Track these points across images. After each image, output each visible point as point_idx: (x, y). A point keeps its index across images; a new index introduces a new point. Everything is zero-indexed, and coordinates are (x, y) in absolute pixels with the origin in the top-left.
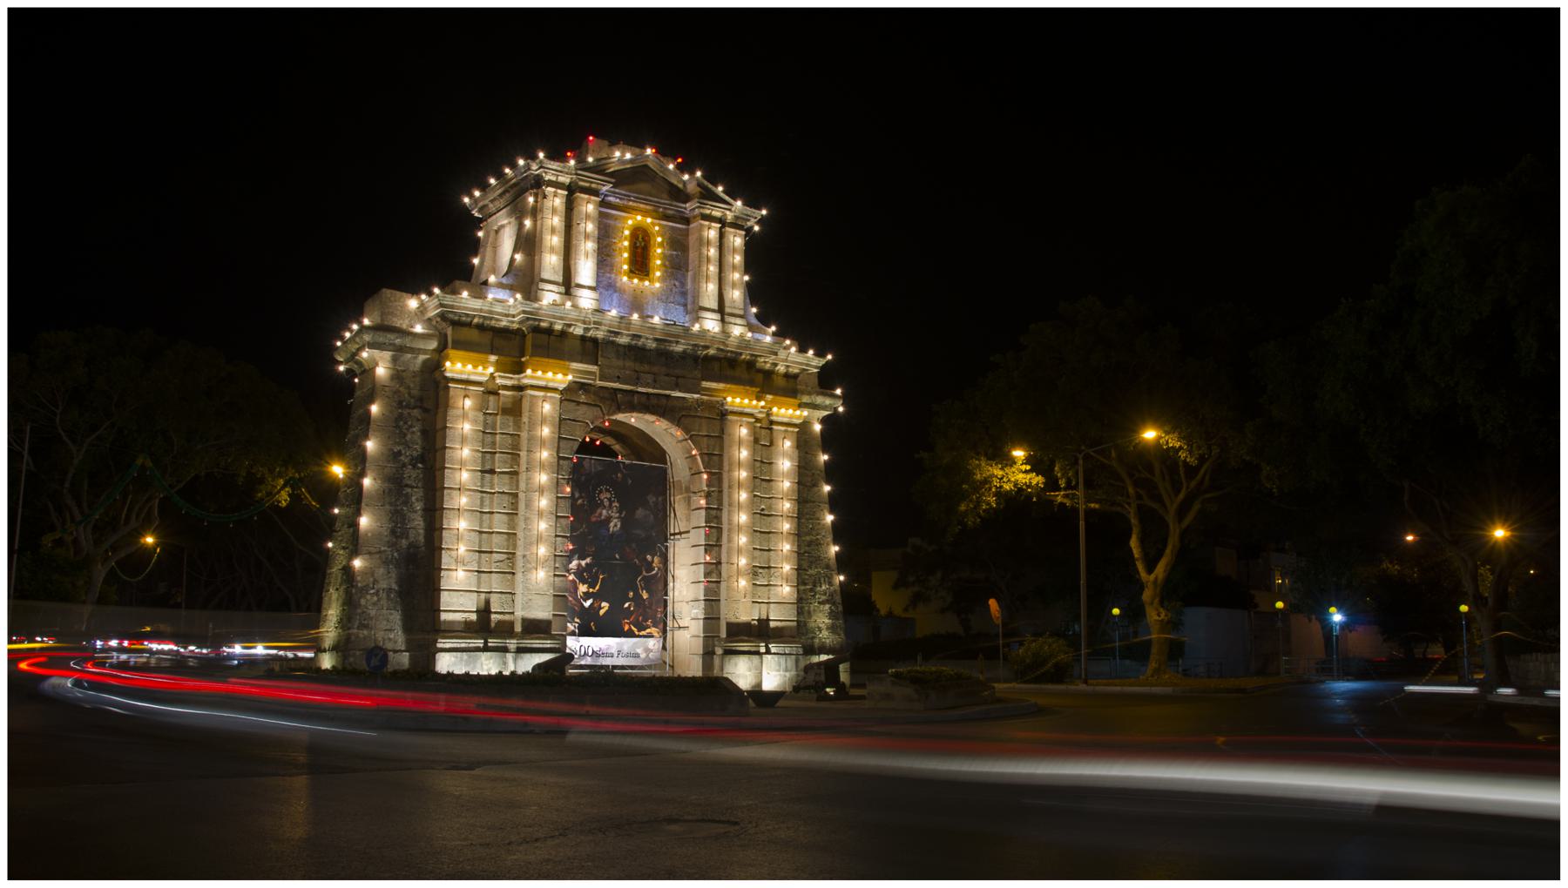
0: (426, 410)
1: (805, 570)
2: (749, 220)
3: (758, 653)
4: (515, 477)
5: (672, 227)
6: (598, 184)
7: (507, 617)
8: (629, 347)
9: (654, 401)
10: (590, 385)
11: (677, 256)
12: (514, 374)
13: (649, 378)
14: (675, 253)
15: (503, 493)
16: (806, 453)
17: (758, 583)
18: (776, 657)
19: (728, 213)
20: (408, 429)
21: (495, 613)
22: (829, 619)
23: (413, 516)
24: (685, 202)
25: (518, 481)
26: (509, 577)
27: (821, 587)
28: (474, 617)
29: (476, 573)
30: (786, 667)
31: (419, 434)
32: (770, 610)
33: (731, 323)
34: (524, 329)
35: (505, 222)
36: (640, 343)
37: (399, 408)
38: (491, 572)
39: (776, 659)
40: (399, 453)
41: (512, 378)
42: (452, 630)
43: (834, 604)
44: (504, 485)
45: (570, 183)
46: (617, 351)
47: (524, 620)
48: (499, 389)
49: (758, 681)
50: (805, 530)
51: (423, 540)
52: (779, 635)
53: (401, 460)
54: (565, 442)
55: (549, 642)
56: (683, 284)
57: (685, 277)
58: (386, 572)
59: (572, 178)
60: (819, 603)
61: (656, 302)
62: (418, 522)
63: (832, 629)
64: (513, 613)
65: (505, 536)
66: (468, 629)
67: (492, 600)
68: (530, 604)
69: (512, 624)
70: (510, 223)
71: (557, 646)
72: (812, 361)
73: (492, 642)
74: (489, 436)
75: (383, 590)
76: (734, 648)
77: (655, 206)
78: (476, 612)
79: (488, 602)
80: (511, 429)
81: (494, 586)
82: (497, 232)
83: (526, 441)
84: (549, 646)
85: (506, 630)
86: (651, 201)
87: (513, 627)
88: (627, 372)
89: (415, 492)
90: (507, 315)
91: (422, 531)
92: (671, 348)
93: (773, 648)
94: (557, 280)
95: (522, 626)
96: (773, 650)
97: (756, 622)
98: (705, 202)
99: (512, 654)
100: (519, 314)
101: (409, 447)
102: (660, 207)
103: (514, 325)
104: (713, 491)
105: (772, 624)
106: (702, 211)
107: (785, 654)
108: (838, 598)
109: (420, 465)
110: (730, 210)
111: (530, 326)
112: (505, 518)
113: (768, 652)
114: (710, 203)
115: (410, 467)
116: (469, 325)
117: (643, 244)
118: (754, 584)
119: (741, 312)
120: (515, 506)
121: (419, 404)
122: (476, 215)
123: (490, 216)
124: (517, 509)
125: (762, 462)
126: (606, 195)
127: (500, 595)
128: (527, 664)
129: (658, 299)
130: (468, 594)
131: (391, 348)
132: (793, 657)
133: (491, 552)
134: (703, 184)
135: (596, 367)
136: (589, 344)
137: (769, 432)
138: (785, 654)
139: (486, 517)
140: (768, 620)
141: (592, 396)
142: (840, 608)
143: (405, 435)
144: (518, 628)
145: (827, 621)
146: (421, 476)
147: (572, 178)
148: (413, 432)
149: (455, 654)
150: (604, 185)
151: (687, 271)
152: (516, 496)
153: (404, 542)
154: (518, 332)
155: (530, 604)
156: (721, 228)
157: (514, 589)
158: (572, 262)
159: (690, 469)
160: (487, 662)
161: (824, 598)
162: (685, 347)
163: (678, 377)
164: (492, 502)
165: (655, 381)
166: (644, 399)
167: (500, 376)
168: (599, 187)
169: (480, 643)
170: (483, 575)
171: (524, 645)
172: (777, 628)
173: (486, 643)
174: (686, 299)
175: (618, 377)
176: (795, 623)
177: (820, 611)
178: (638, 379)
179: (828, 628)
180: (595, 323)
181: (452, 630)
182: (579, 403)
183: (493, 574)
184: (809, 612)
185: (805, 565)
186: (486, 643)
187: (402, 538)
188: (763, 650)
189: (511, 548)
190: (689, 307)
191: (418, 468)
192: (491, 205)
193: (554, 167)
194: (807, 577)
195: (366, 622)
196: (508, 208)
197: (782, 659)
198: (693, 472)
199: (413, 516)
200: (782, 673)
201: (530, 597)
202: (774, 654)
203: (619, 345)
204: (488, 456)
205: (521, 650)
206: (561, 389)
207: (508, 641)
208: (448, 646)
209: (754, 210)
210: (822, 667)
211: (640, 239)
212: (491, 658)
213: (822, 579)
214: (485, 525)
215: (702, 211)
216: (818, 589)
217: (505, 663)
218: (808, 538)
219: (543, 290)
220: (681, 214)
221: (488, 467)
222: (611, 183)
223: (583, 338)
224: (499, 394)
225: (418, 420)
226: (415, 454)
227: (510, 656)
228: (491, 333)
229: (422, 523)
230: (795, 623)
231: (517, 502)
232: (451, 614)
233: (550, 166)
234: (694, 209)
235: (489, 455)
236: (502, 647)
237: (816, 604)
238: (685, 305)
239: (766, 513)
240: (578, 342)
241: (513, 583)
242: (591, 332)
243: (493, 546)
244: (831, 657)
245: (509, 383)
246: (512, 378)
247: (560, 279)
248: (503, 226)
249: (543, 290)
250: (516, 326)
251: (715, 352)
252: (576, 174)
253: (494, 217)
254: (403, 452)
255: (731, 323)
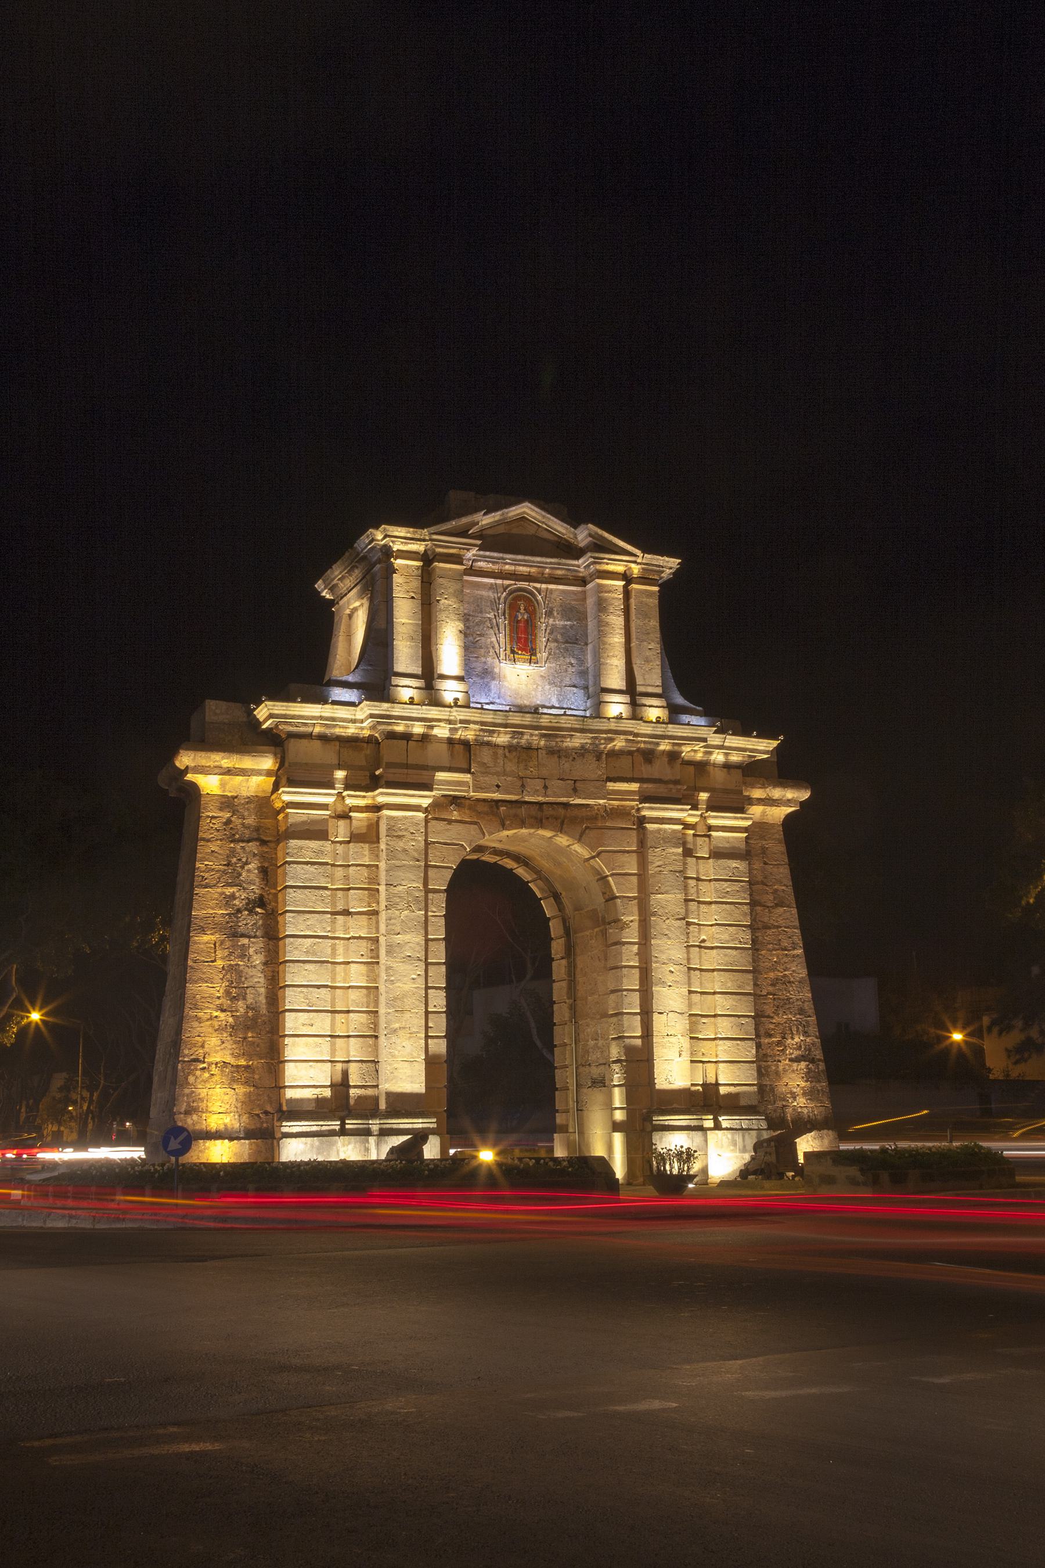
0: (263, 843)
1: (769, 1017)
2: (663, 572)
3: (700, 1128)
4: (374, 917)
5: (563, 591)
6: (460, 548)
7: (370, 1092)
8: (511, 748)
9: (548, 811)
10: (464, 797)
11: (571, 627)
12: (367, 792)
13: (538, 784)
14: (569, 623)
15: (360, 938)
16: (765, 863)
17: (700, 1036)
18: (728, 1134)
19: (633, 565)
20: (242, 867)
21: (355, 1087)
22: (807, 1081)
23: (251, 972)
24: (578, 558)
25: (377, 922)
26: (371, 1041)
27: (793, 1039)
28: (327, 1093)
29: (329, 1039)
30: (744, 1147)
31: (256, 871)
32: (719, 1072)
33: (645, 706)
34: (377, 735)
35: (357, 604)
36: (523, 741)
37: (231, 842)
38: (349, 1036)
39: (730, 1136)
40: (233, 897)
41: (364, 797)
42: (297, 1111)
43: (812, 1061)
44: (361, 927)
45: (425, 550)
46: (495, 754)
47: (389, 1095)
48: (350, 812)
49: (704, 1164)
50: (768, 964)
51: (264, 1001)
52: (732, 1105)
53: (235, 905)
54: (435, 870)
55: (420, 1120)
56: (581, 662)
57: (583, 652)
58: (219, 1043)
59: (426, 545)
60: (791, 1060)
61: (548, 687)
62: (257, 978)
63: (810, 1094)
64: (377, 1086)
65: (364, 991)
66: (318, 1110)
67: (350, 1071)
68: (395, 1074)
69: (376, 1099)
70: (362, 605)
71: (431, 1126)
72: (763, 747)
73: (351, 1124)
74: (340, 869)
75: (216, 1064)
76: (667, 1123)
77: (539, 567)
78: (329, 1086)
79: (345, 1074)
80: (367, 860)
81: (352, 1053)
82: (350, 616)
83: (384, 873)
84: (420, 1126)
85: (368, 1108)
86: (534, 562)
87: (377, 1104)
88: (509, 779)
89: (253, 943)
90: (354, 721)
91: (262, 990)
92: (565, 744)
93: (725, 1121)
94: (415, 672)
95: (387, 1103)
96: (725, 1124)
97: (700, 1088)
98: (602, 555)
99: (375, 1138)
100: (367, 718)
101: (244, 889)
102: (546, 568)
103: (365, 732)
104: (632, 921)
105: (723, 1090)
106: (598, 567)
107: (742, 1129)
108: (818, 1054)
109: (258, 910)
110: (635, 562)
111: (382, 733)
112: (363, 968)
113: (717, 1127)
114: (607, 556)
115: (246, 913)
116: (309, 736)
117: (525, 617)
118: (691, 1038)
119: (659, 690)
120: (375, 953)
121: (255, 835)
122: (328, 596)
123: (342, 598)
124: (378, 957)
125: (698, 879)
126: (474, 561)
127: (359, 1064)
128: (377, 1151)
129: (550, 684)
130: (319, 1064)
131: (217, 771)
132: (754, 1133)
133: (348, 1012)
134: (597, 533)
135: (469, 776)
136: (459, 748)
137: (707, 839)
138: (742, 1129)
139: (339, 968)
140: (717, 1084)
141: (467, 811)
142: (822, 1066)
143: (240, 875)
144: (383, 1106)
145: (803, 1084)
146: (260, 922)
147: (426, 545)
148: (249, 871)
149: (303, 1139)
150: (468, 550)
151: (586, 644)
152: (376, 940)
153: (241, 1004)
154: (370, 740)
155: (395, 1074)
156: (625, 587)
157: (377, 1056)
158: (433, 649)
159: (604, 893)
160: (345, 1148)
161: (797, 1053)
162: (583, 741)
163: (575, 781)
164: (347, 949)
165: (546, 787)
166: (534, 810)
167: (349, 796)
168: (462, 552)
169: (335, 1125)
170: (338, 1040)
171: (388, 1126)
172: (729, 1095)
173: (343, 1124)
174: (587, 680)
175: (498, 786)
176: (755, 1088)
177: (793, 1071)
178: (523, 786)
179: (804, 1094)
180: (462, 722)
181: (297, 1111)
182: (450, 822)
183: (351, 1039)
184: (777, 1073)
185: (769, 1010)
186: (343, 1124)
187: (238, 1000)
188: (709, 1123)
189: (372, 1005)
190: (591, 689)
191: (257, 914)
192: (341, 585)
193: (402, 534)
194: (772, 1026)
195: (195, 1104)
196: (358, 587)
197: (738, 1137)
198: (607, 897)
199: (251, 972)
200: (738, 1154)
201: (396, 1066)
202: (727, 1129)
203: (496, 746)
204: (340, 894)
205: (384, 1133)
206: (425, 806)
207: (370, 1122)
208: (295, 1130)
209: (667, 559)
210: (773, 1144)
211: (522, 611)
212: (349, 1143)
213: (794, 1029)
214: (339, 978)
215: (598, 567)
216: (789, 1041)
217: (367, 1150)
218: (772, 975)
219: (397, 686)
220: (574, 574)
221: (340, 907)
222: (475, 545)
223: (450, 741)
224: (350, 818)
225: (255, 855)
226: (252, 896)
227: (372, 1140)
228: (338, 743)
229: (262, 980)
230: (755, 1088)
231: (378, 948)
232: (299, 1090)
233: (396, 534)
234: (588, 566)
235: (341, 892)
236: (364, 1129)
237: (787, 1062)
238: (586, 688)
239: (708, 944)
240: (445, 746)
241: (376, 1048)
242: (460, 732)
243: (350, 1003)
244: (410, 1137)
245: (362, 802)
246: (364, 797)
247: (418, 671)
248: (355, 609)
249: (397, 686)
250: (366, 733)
251: (624, 744)
252: (431, 540)
253: (345, 599)
254: (237, 894)
255: (645, 706)
